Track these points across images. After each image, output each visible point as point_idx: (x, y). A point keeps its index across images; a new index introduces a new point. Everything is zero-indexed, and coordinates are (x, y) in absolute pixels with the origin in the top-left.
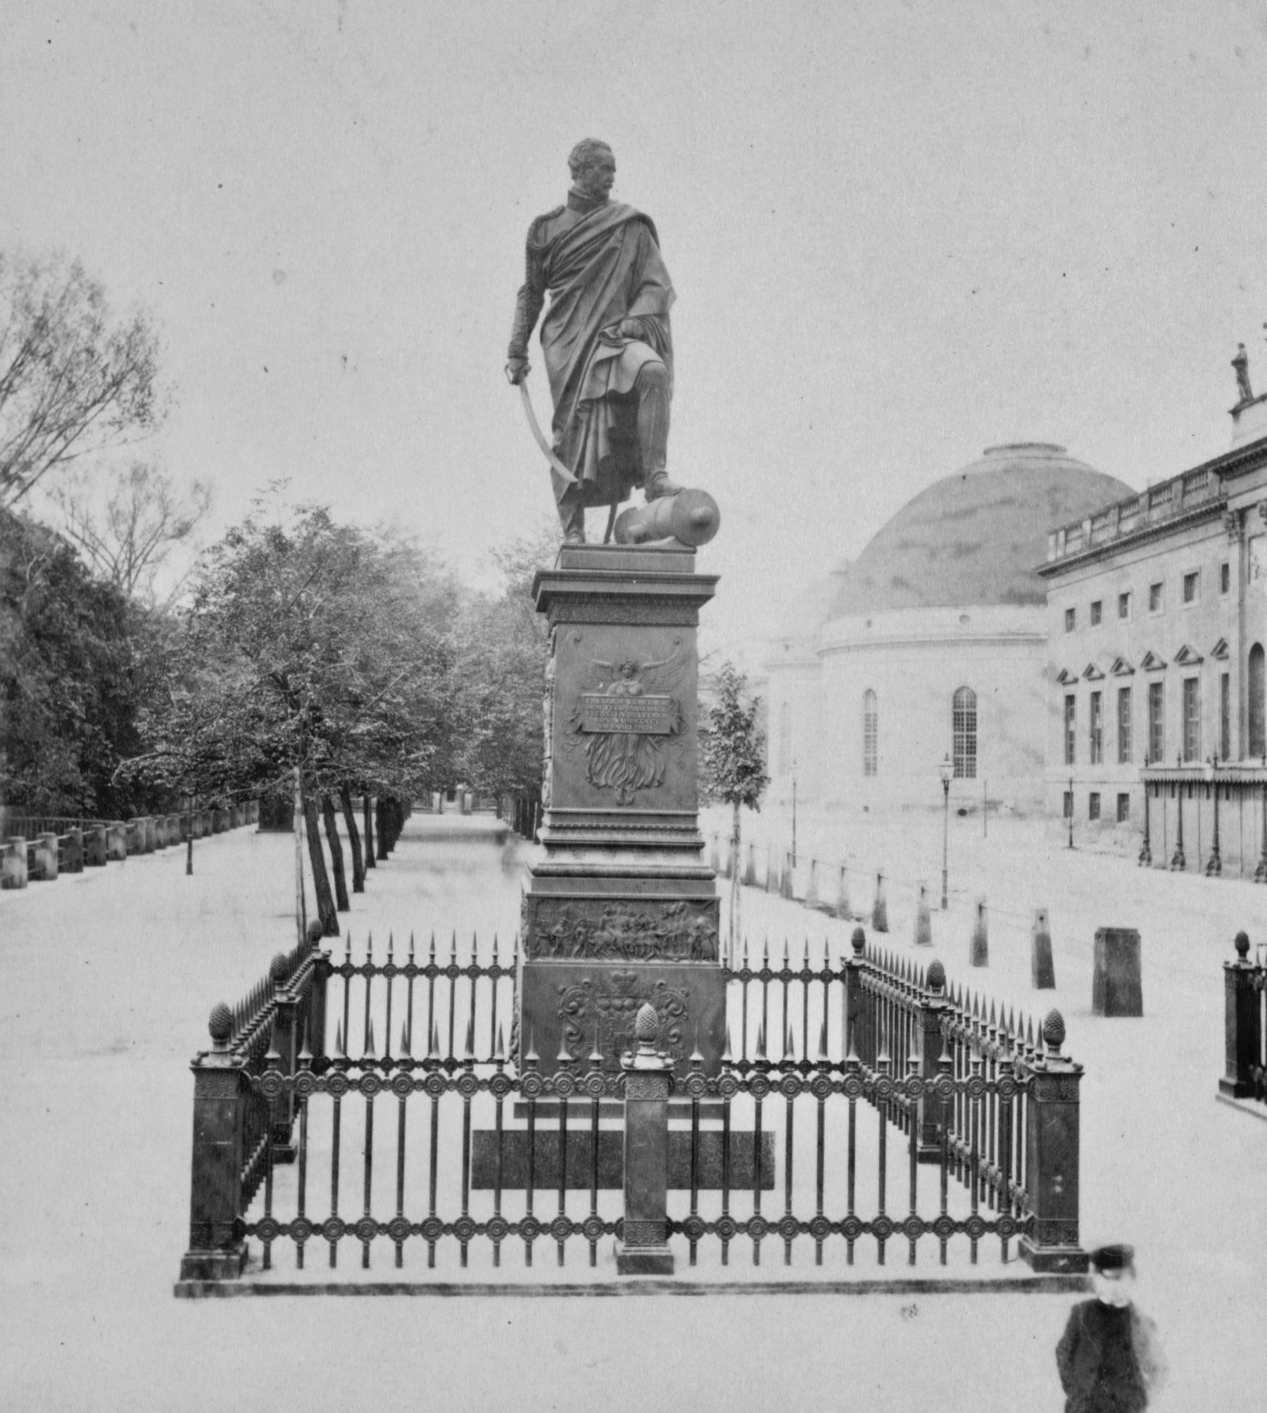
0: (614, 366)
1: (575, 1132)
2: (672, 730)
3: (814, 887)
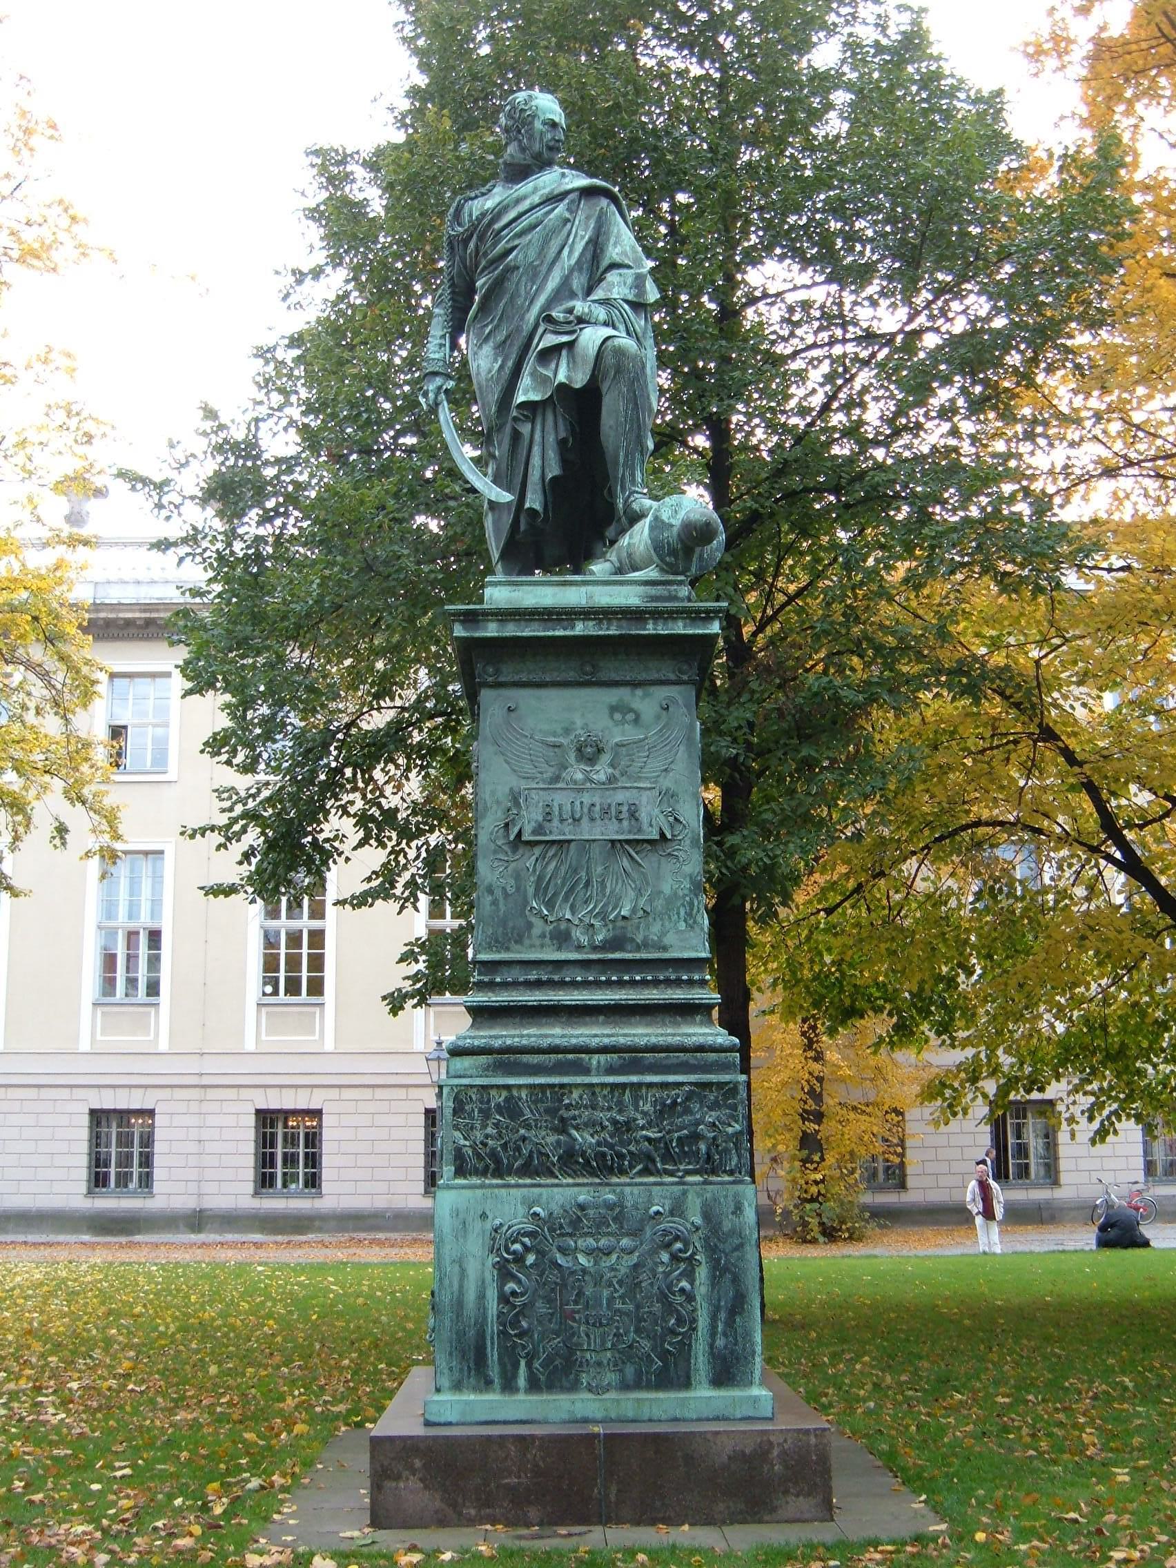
0: (564, 353)
2: (662, 835)
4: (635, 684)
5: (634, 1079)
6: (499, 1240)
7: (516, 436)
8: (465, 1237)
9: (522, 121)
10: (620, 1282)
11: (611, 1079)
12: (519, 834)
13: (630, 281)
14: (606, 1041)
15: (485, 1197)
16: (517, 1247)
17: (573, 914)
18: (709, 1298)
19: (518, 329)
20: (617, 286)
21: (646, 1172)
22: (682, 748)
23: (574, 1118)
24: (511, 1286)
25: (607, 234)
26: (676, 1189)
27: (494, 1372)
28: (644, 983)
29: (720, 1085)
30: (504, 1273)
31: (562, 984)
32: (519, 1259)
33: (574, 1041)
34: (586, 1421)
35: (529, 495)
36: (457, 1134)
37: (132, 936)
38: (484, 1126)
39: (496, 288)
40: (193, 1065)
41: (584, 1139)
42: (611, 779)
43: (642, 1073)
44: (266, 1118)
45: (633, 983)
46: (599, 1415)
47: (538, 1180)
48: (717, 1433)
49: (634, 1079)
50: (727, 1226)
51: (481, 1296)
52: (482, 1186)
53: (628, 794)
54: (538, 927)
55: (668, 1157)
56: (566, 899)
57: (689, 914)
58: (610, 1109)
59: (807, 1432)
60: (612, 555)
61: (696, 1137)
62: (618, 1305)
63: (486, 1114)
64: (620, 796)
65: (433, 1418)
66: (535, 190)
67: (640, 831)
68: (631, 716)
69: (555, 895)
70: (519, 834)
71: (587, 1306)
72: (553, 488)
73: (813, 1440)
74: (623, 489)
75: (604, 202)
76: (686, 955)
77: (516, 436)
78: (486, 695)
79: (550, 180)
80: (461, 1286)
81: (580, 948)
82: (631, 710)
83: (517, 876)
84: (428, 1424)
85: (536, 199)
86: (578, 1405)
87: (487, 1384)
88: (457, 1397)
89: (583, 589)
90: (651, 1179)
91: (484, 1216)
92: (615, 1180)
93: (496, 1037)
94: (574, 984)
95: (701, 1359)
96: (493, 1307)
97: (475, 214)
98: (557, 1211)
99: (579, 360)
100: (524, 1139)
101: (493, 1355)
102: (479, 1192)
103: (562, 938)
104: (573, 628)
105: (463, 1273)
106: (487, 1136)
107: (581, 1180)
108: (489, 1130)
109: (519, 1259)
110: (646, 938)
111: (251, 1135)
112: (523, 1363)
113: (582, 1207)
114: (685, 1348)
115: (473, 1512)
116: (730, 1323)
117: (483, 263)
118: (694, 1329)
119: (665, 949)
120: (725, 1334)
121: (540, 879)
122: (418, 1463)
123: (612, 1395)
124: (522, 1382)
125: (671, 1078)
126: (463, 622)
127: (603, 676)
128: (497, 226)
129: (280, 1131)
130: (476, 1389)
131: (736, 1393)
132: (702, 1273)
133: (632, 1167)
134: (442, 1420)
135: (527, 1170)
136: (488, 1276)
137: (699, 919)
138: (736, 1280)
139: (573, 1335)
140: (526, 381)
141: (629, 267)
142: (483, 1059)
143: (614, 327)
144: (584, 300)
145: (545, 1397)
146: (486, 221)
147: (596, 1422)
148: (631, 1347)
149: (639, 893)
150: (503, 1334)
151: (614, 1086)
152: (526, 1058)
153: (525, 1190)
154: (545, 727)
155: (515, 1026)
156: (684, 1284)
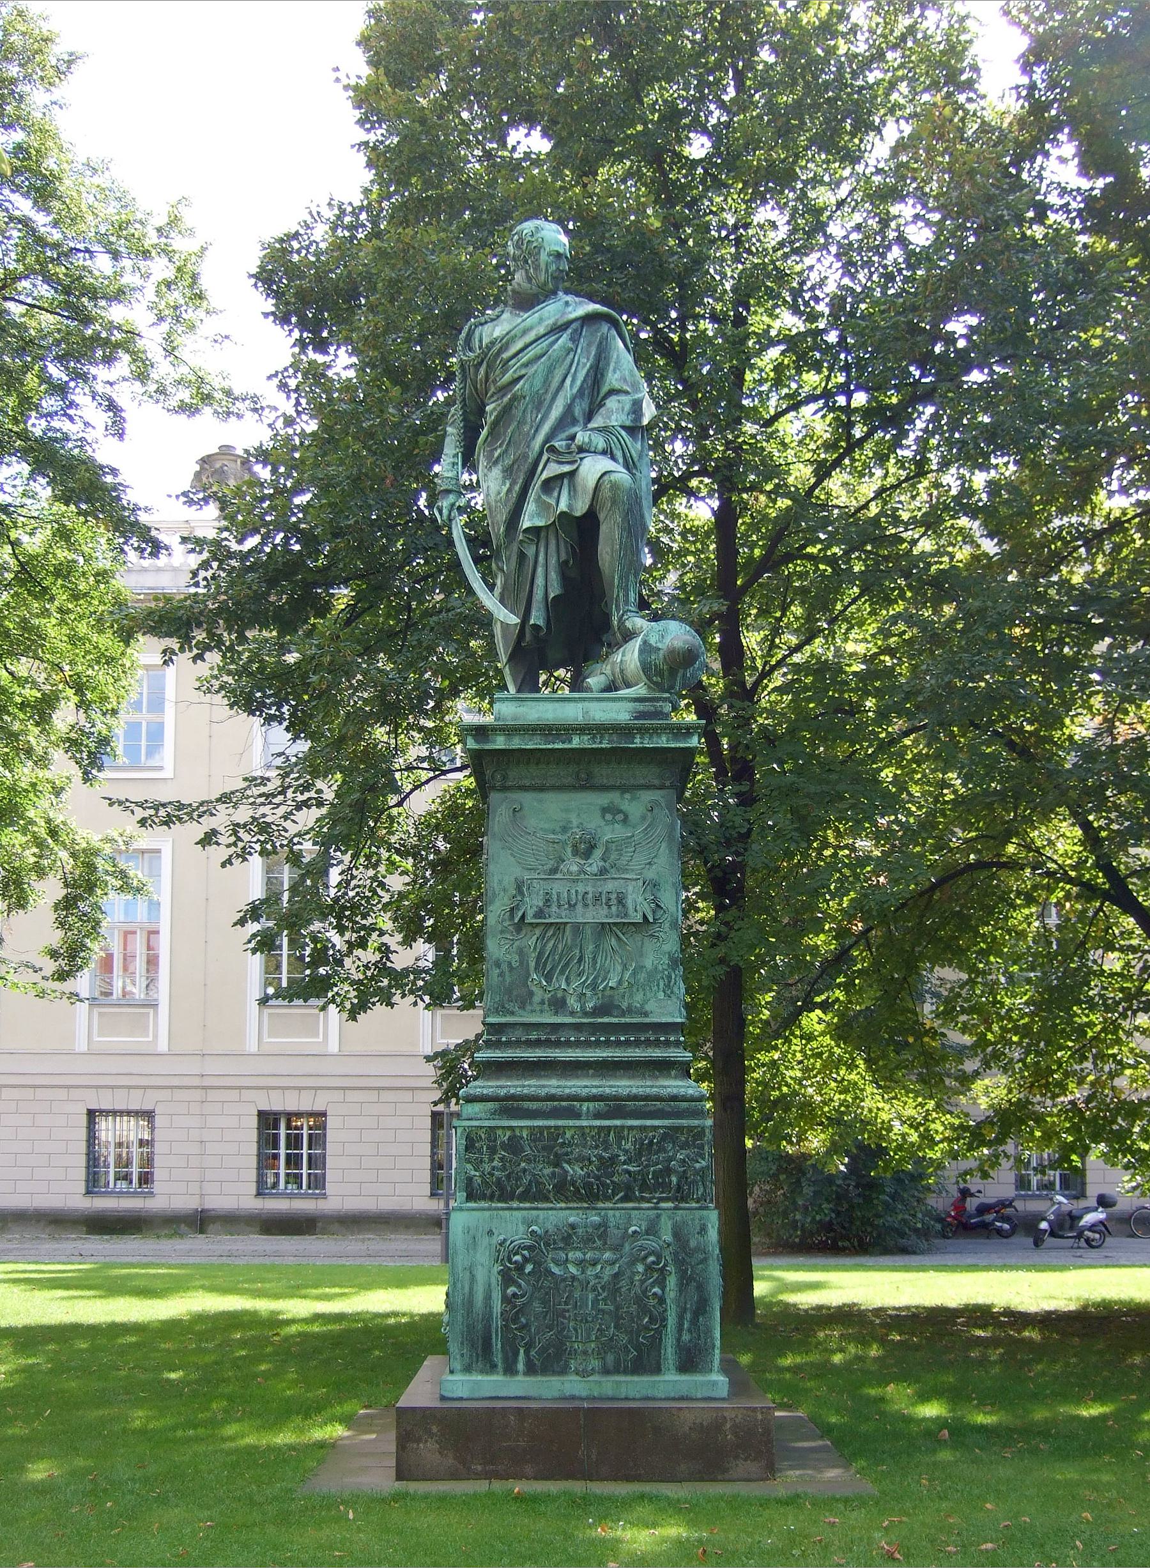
0: (566, 481)
1: (164, 676)
2: (645, 917)
3: (161, 621)
4: (623, 789)
5: (618, 1122)
6: (504, 1254)
7: (522, 556)
8: (475, 1249)
9: (530, 252)
10: (603, 1288)
11: (597, 1123)
12: (523, 917)
13: (627, 407)
14: (594, 1091)
15: (491, 1217)
16: (518, 1258)
17: (568, 984)
18: (677, 1301)
19: (525, 456)
20: (615, 413)
21: (626, 1199)
22: (664, 845)
23: (567, 1154)
24: (511, 1290)
25: (607, 360)
26: (652, 1213)
27: (498, 1358)
28: (627, 1043)
29: (690, 1129)
30: (507, 1278)
31: (558, 1044)
32: (520, 1268)
33: (567, 1091)
34: (573, 1398)
35: (534, 613)
36: (469, 1166)
37: (127, 934)
38: (492, 1160)
39: (506, 412)
40: (192, 1067)
41: (574, 1171)
42: (603, 871)
43: (624, 1118)
44: (268, 1120)
45: (618, 1044)
46: (584, 1394)
47: (536, 1205)
49: (618, 1122)
50: (693, 1244)
51: (488, 1297)
52: (489, 1209)
53: (616, 883)
54: (538, 995)
55: (644, 1187)
56: (562, 972)
57: (668, 986)
58: (597, 1147)
59: (754, 1409)
60: (607, 669)
61: (668, 1171)
62: (602, 1306)
63: (493, 1150)
64: (610, 886)
65: (446, 1394)
66: (541, 320)
67: (626, 915)
68: (620, 817)
69: (553, 969)
70: (523, 917)
71: (575, 1307)
72: (554, 607)
73: (760, 1417)
74: (618, 610)
75: (605, 327)
76: (664, 1020)
77: (522, 556)
78: (494, 797)
79: (552, 311)
80: (471, 1289)
81: (572, 1013)
82: (620, 811)
83: (521, 952)
84: (443, 1398)
85: (542, 330)
86: (567, 1385)
87: (492, 1368)
88: (467, 1377)
89: (580, 705)
90: (631, 1205)
91: (490, 1233)
92: (600, 1205)
93: (502, 1087)
94: (568, 1044)
95: (669, 1350)
96: (497, 1306)
98: (551, 1229)
99: (579, 489)
100: (524, 1171)
101: (497, 1345)
102: (487, 1214)
103: (559, 1004)
104: (570, 741)
105: (473, 1279)
106: (493, 1168)
107: (571, 1205)
108: (495, 1163)
109: (520, 1268)
110: (630, 1006)
111: (253, 1135)
112: (522, 1351)
113: (573, 1226)
114: (656, 1342)
115: (479, 1468)
116: (694, 1322)
117: (493, 390)
118: (665, 1326)
119: (646, 1014)
120: (689, 1331)
121: (539, 958)
122: (435, 1429)
123: (595, 1378)
124: (521, 1366)
125: (649, 1123)
126: (474, 737)
127: (598, 781)
128: (505, 355)
129: (283, 1132)
130: (482, 1372)
131: (698, 1378)
132: (672, 1281)
133: (614, 1194)
134: (455, 1395)
135: (524, 1197)
136: (494, 1281)
137: (676, 990)
138: (700, 1288)
139: (563, 1329)
140: (530, 507)
141: (627, 393)
142: (490, 1105)
143: (613, 458)
144: (585, 429)
145: (539, 1378)
146: (498, 346)
147: (581, 1399)
148: (611, 1339)
149: (625, 967)
150: (506, 1327)
151: (601, 1128)
152: (527, 1105)
153: (525, 1213)
154: (546, 826)
155: (518, 1078)
156: (656, 1290)
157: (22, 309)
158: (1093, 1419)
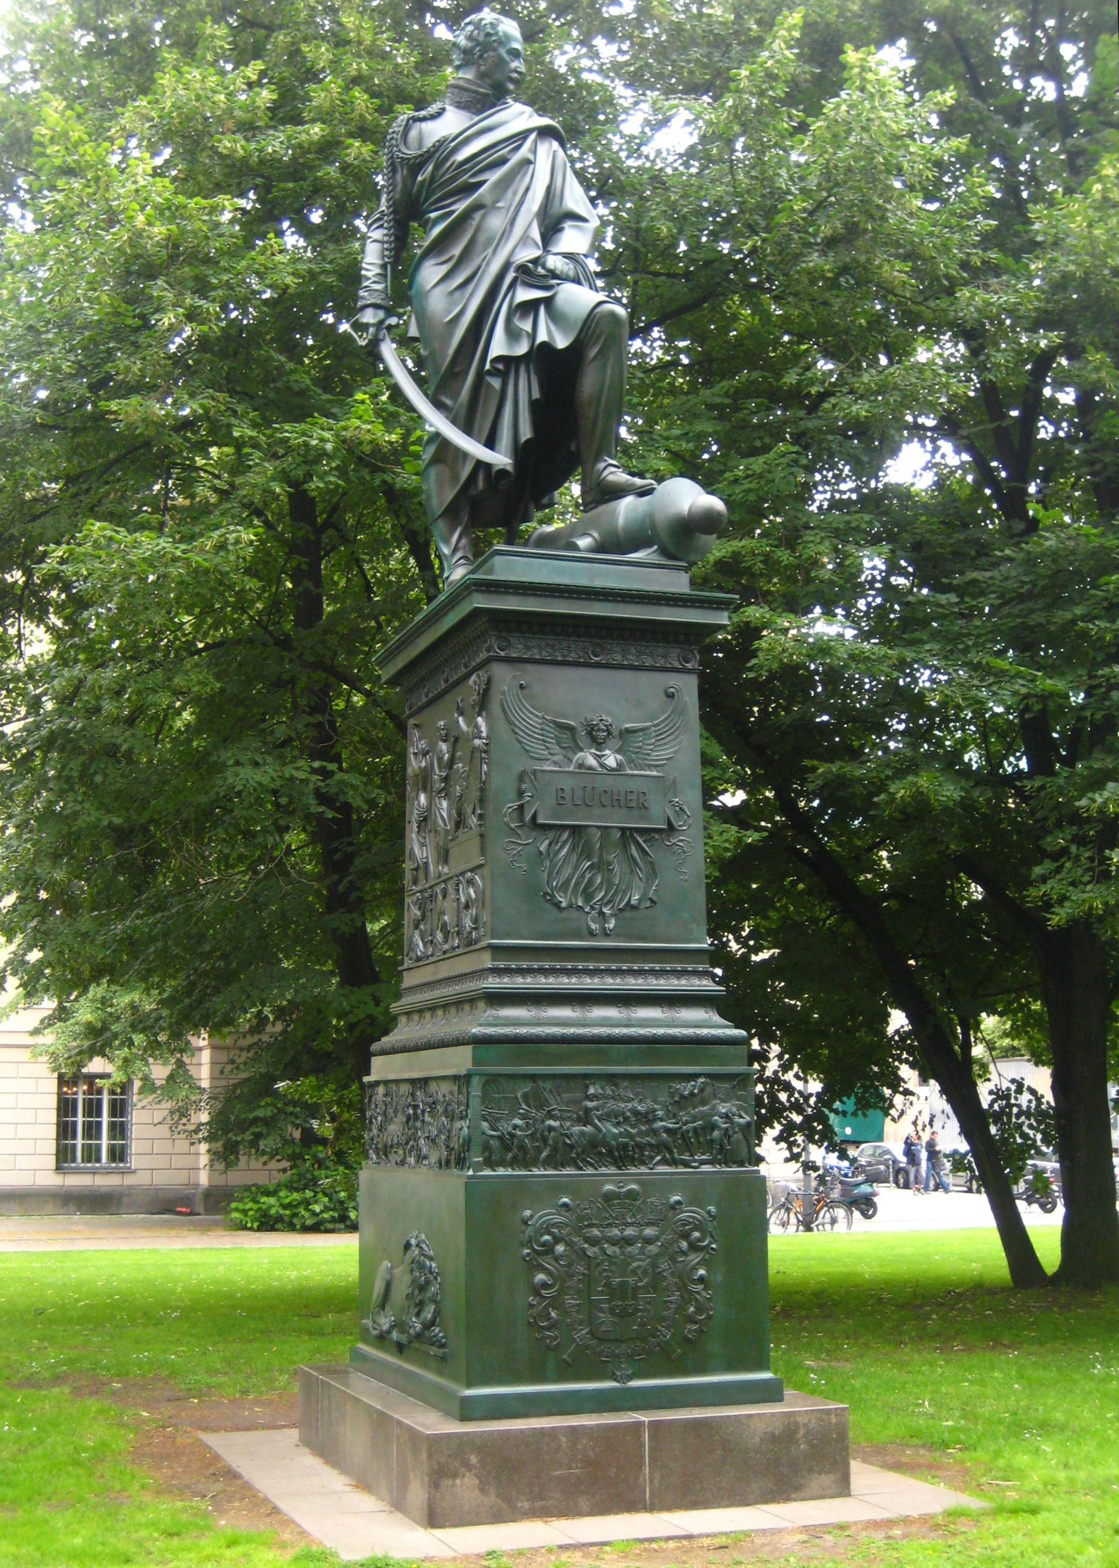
2: (670, 823)
12: (534, 817)
36: (485, 1124)
48: (751, 1416)
59: (828, 1412)
97: (429, 143)
115: (526, 1505)
122: (474, 1459)
157: (1030, 1215)
158: (764, 961)
